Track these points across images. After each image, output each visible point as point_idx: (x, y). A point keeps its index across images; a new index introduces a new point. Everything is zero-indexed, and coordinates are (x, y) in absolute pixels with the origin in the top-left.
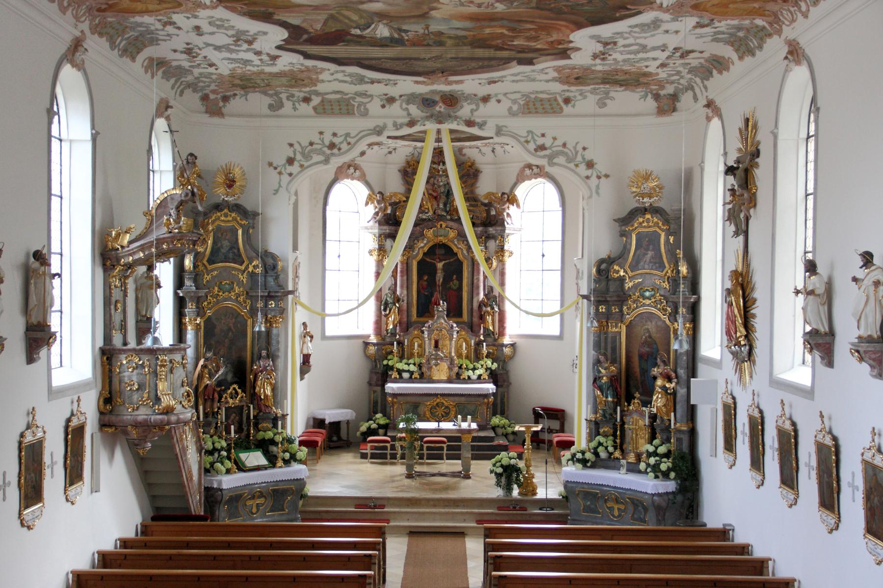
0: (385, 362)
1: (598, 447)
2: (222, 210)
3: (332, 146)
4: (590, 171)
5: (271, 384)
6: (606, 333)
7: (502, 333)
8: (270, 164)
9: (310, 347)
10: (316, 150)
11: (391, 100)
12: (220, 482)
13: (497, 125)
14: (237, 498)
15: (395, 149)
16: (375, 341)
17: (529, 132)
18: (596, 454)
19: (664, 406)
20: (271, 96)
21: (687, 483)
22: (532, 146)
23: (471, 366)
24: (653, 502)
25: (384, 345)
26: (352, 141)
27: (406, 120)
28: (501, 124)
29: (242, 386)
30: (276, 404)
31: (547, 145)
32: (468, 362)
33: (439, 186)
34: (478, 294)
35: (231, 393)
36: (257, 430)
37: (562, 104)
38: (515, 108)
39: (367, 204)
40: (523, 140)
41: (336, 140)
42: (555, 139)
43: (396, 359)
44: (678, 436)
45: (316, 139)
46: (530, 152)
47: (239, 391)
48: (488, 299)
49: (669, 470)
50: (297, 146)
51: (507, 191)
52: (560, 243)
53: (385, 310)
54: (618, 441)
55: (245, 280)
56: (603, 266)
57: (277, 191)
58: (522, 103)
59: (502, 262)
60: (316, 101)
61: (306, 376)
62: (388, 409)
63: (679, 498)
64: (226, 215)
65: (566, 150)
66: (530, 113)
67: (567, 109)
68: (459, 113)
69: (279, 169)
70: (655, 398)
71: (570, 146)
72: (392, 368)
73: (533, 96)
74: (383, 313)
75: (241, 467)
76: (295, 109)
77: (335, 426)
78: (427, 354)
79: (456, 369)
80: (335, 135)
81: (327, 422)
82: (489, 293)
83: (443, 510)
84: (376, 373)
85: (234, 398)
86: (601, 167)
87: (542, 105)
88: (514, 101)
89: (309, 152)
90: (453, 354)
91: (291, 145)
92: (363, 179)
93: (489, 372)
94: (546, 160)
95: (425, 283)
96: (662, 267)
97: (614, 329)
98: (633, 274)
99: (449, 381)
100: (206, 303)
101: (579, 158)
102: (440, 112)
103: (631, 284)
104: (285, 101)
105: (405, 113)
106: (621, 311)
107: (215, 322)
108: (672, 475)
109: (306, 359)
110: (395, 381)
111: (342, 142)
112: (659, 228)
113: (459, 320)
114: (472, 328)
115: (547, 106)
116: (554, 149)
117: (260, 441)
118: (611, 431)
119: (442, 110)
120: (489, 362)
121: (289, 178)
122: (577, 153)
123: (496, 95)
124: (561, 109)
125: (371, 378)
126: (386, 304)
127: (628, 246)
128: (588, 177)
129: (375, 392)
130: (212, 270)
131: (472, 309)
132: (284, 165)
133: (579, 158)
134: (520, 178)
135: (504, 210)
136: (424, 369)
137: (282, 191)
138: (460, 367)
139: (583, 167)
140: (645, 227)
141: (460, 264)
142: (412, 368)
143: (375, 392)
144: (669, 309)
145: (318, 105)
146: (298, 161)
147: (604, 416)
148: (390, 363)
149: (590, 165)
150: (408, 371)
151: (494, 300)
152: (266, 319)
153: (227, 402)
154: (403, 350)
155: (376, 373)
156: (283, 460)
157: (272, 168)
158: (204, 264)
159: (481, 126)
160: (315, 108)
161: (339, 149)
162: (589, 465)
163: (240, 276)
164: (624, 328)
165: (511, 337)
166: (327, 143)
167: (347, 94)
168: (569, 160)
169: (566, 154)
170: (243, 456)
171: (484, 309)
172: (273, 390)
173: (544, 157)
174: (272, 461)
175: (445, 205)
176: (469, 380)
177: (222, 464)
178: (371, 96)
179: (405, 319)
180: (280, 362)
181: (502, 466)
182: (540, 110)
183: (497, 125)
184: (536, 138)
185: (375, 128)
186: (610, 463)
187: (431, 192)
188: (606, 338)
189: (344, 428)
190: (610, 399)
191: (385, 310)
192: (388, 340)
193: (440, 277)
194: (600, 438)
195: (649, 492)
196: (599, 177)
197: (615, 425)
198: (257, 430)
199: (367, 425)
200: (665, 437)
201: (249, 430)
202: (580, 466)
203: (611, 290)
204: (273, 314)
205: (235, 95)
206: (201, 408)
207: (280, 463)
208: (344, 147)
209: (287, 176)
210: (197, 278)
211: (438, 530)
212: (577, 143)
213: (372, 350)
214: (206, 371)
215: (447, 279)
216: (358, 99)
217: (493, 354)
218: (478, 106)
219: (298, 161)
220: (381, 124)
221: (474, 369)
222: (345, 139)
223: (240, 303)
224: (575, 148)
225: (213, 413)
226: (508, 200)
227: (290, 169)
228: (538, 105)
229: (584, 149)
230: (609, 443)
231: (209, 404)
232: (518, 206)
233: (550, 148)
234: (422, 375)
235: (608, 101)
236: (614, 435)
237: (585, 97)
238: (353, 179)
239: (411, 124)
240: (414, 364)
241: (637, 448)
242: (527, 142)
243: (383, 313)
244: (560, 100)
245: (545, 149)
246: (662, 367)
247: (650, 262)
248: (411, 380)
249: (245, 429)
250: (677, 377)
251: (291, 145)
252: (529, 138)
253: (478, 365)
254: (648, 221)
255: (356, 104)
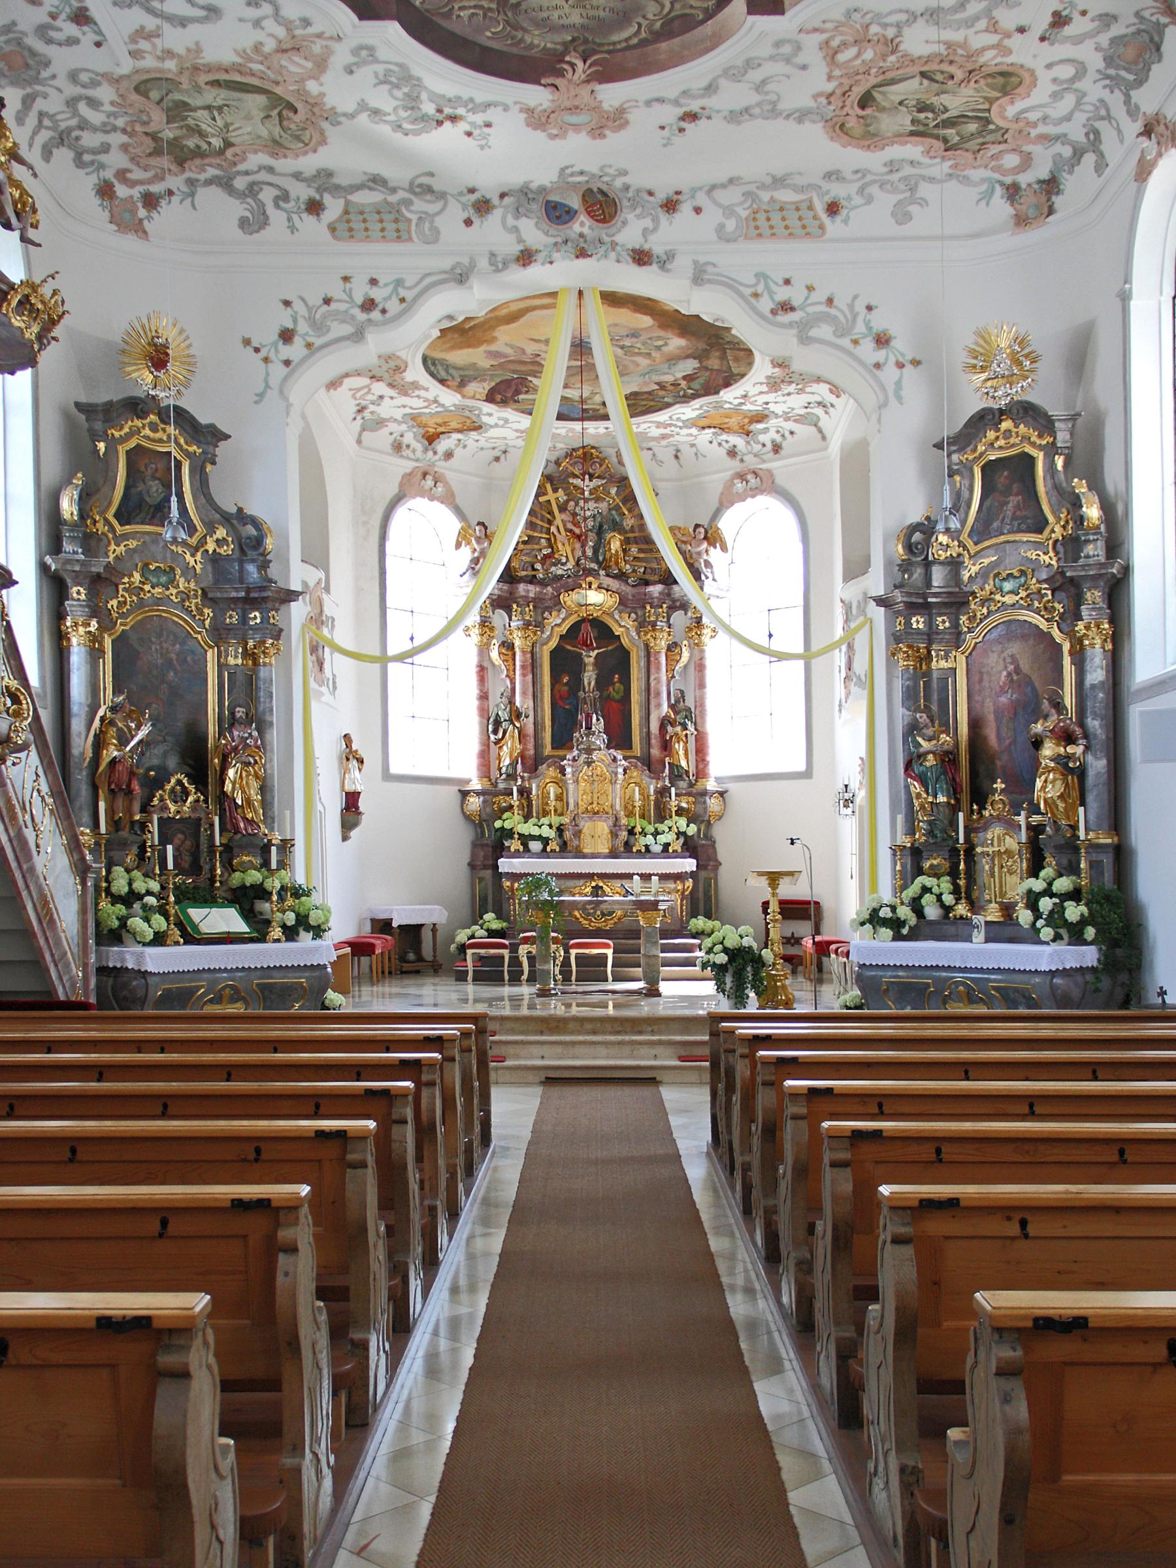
0: (498, 824)
1: (921, 896)
2: (142, 415)
3: (369, 305)
4: (883, 352)
5: (257, 776)
6: (928, 673)
7: (701, 773)
8: (247, 342)
9: (357, 780)
10: (337, 312)
11: (483, 207)
12: (140, 957)
13: (695, 262)
14: (179, 994)
15: (505, 452)
16: (479, 787)
17: (761, 276)
18: (918, 911)
19: (1061, 797)
20: (241, 195)
21: (1119, 952)
22: (765, 305)
23: (650, 829)
24: (1053, 987)
25: (496, 795)
26: (409, 295)
27: (517, 249)
28: (702, 259)
29: (199, 775)
30: (269, 819)
31: (795, 304)
32: (645, 823)
33: (585, 519)
34: (659, 705)
35: (173, 790)
36: (230, 868)
37: (823, 216)
38: (731, 225)
39: (458, 546)
40: (747, 292)
41: (377, 294)
42: (810, 288)
43: (517, 818)
44: (1094, 857)
45: (336, 290)
46: (762, 316)
47: (192, 788)
48: (676, 713)
49: (1084, 922)
50: (298, 306)
51: (705, 522)
52: (801, 609)
53: (495, 732)
54: (962, 882)
55: (198, 567)
56: (917, 536)
57: (261, 396)
58: (744, 214)
59: (697, 646)
60: (333, 208)
61: (353, 834)
62: (505, 906)
63: (1105, 983)
64: (154, 428)
65: (833, 311)
66: (760, 235)
67: (834, 227)
68: (619, 238)
69: (263, 353)
70: (1039, 783)
71: (841, 302)
72: (510, 833)
73: (765, 196)
74: (492, 737)
75: (191, 936)
76: (293, 229)
77: (412, 932)
78: (571, 806)
79: (624, 834)
80: (373, 282)
81: (395, 925)
82: (677, 701)
83: (612, 1038)
84: (483, 846)
85: (178, 802)
86: (902, 346)
87: (784, 219)
88: (729, 211)
89: (324, 317)
90: (618, 808)
91: (287, 303)
92: (449, 500)
93: (682, 840)
94: (794, 331)
95: (566, 688)
96: (1040, 525)
97: (943, 664)
98: (980, 547)
99: (613, 854)
100: (114, 603)
101: (860, 328)
102: (581, 235)
103: (974, 569)
104: (270, 210)
105: (512, 238)
106: (956, 625)
107: (136, 645)
108: (1090, 932)
109: (351, 801)
110: (517, 854)
111: (390, 297)
112: (1033, 444)
113: (628, 754)
114: (649, 764)
115: (794, 222)
116: (810, 310)
117: (234, 890)
118: (946, 865)
119: (586, 230)
120: (682, 822)
121: (285, 370)
122: (855, 316)
123: (694, 191)
124: (822, 227)
125: (473, 855)
126: (498, 723)
127: (966, 494)
128: (878, 366)
129: (481, 879)
130: (126, 537)
131: (649, 733)
132: (275, 345)
133: (860, 328)
134: (727, 500)
135: (699, 554)
136: (568, 835)
137: (272, 395)
138: (631, 832)
139: (868, 345)
140: (1001, 448)
141: (625, 654)
142: (546, 832)
143: (481, 879)
144: (1059, 607)
145: (339, 220)
146: (303, 336)
147: (930, 833)
148: (507, 825)
149: (882, 341)
150: (539, 838)
151: (686, 713)
152: (245, 649)
153: (165, 808)
154: (530, 805)
155: (483, 846)
156: (284, 927)
157: (250, 350)
158: (106, 521)
159: (665, 262)
160: (332, 229)
161: (384, 311)
162: (905, 931)
163: (188, 557)
164: (962, 659)
165: (717, 779)
166: (359, 300)
167: (394, 190)
168: (841, 332)
169: (833, 320)
170: (196, 914)
171: (670, 728)
172: (263, 789)
173: (791, 325)
174: (260, 930)
175: (596, 551)
176: (647, 852)
177: (147, 920)
178: (442, 196)
179: (532, 752)
180: (274, 736)
181: (726, 950)
182: (780, 230)
183: (695, 262)
184: (773, 287)
185: (453, 269)
186: (950, 927)
187: (570, 526)
188: (927, 685)
189: (427, 935)
190: (942, 799)
191: (495, 732)
192: (501, 786)
193: (589, 677)
194: (922, 880)
195: (1044, 967)
196: (900, 366)
197: (954, 852)
198: (230, 868)
199: (468, 932)
200: (1065, 862)
201: (213, 869)
202: (887, 933)
203: (935, 584)
204: (258, 637)
205: (170, 193)
206: (102, 805)
207: (277, 933)
208: (393, 306)
209: (282, 367)
210: (91, 542)
211: (608, 1075)
212: (855, 297)
213: (474, 803)
214: (112, 731)
215: (602, 682)
216: (419, 205)
217: (688, 810)
218: (656, 220)
219: (303, 336)
220: (465, 261)
221: (656, 834)
222: (395, 290)
223: (188, 611)
224: (851, 306)
225: (133, 823)
226: (706, 538)
227: (286, 351)
228: (776, 217)
229: (869, 308)
230: (945, 884)
231: (120, 802)
232: (724, 549)
233: (802, 308)
234: (564, 846)
235: (914, 209)
236: (954, 873)
237: (869, 200)
238: (432, 499)
239: (526, 258)
240: (550, 826)
241: (1003, 895)
242: (756, 295)
243: (492, 737)
244: (820, 208)
245: (792, 309)
246: (1054, 717)
247: (1014, 518)
248: (544, 853)
249: (207, 867)
250: (1086, 736)
251: (287, 303)
252: (760, 289)
253: (662, 827)
254: (1008, 434)
255: (414, 218)
